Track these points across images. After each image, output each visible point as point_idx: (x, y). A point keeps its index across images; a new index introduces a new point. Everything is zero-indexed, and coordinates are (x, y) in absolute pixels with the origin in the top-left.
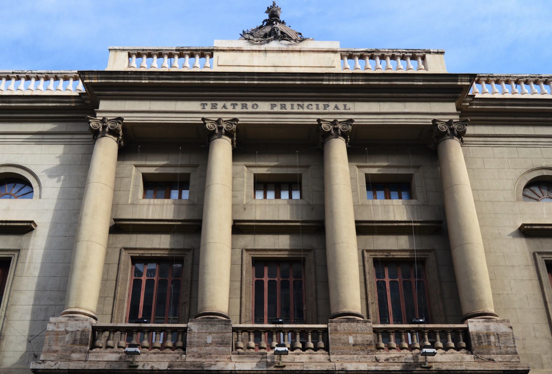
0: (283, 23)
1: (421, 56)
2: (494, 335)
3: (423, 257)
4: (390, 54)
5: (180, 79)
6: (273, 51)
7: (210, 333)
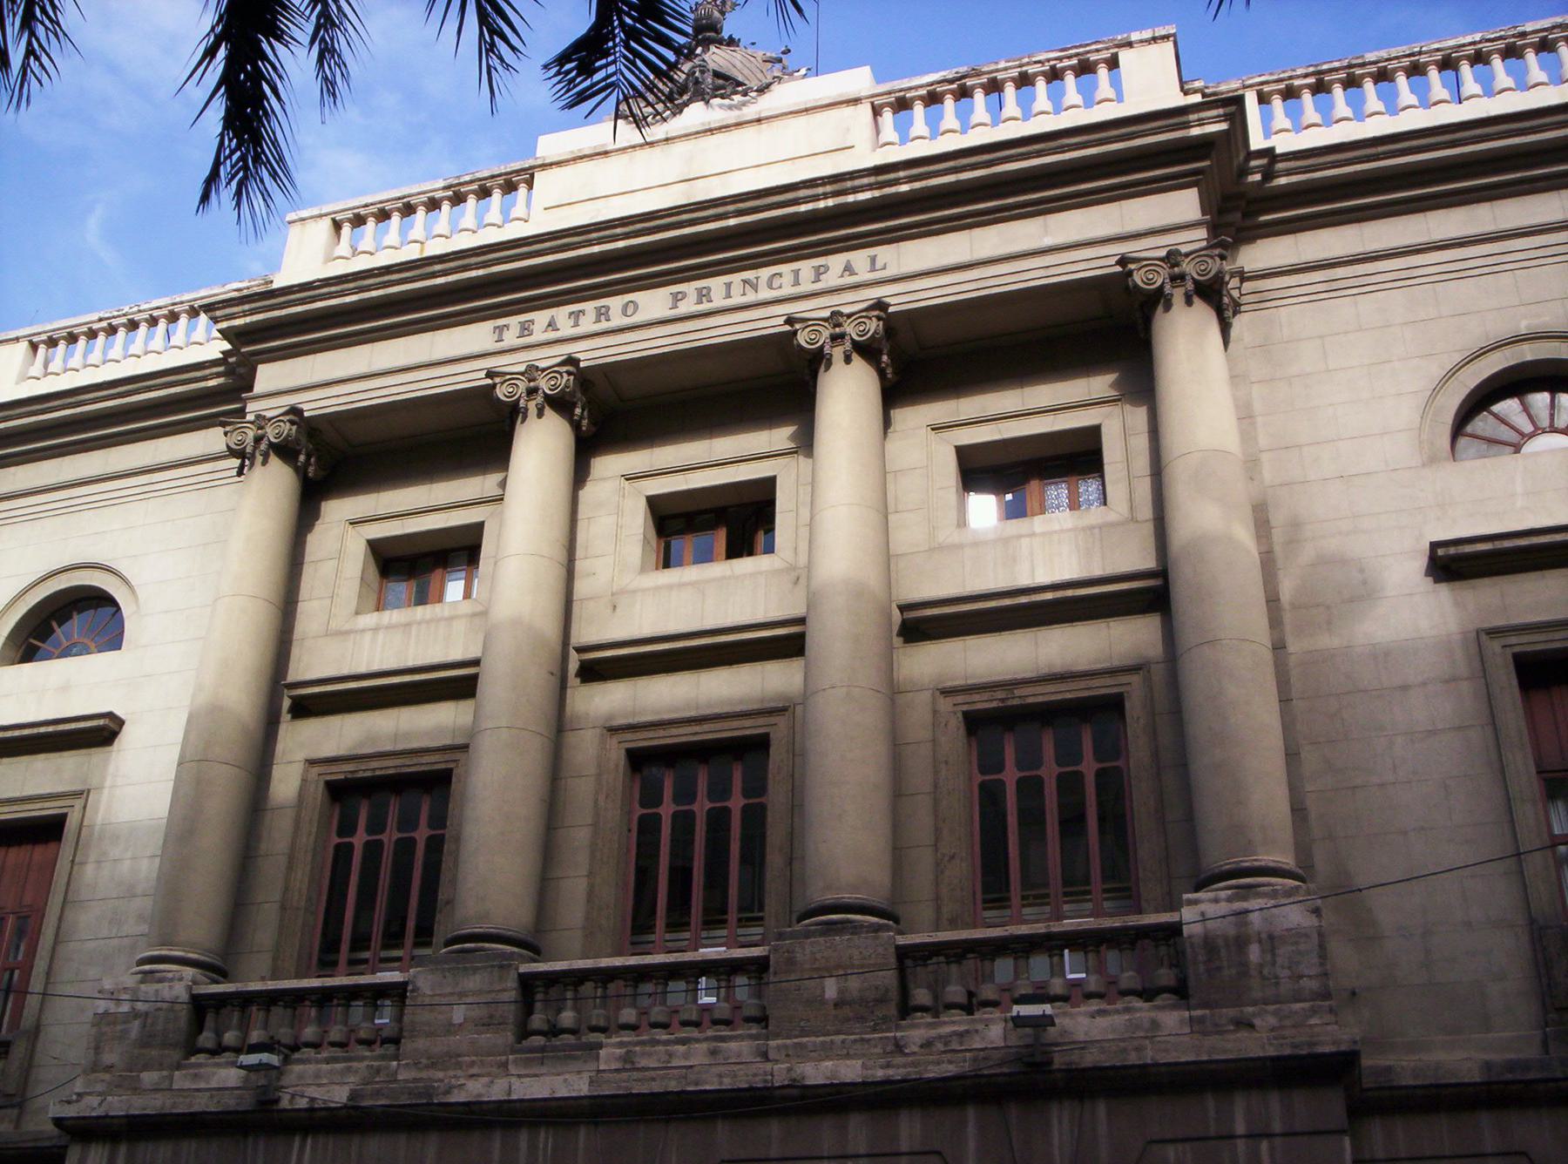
1: (1106, 61)
2: (1260, 942)
3: (443, 766)
5: (434, 275)
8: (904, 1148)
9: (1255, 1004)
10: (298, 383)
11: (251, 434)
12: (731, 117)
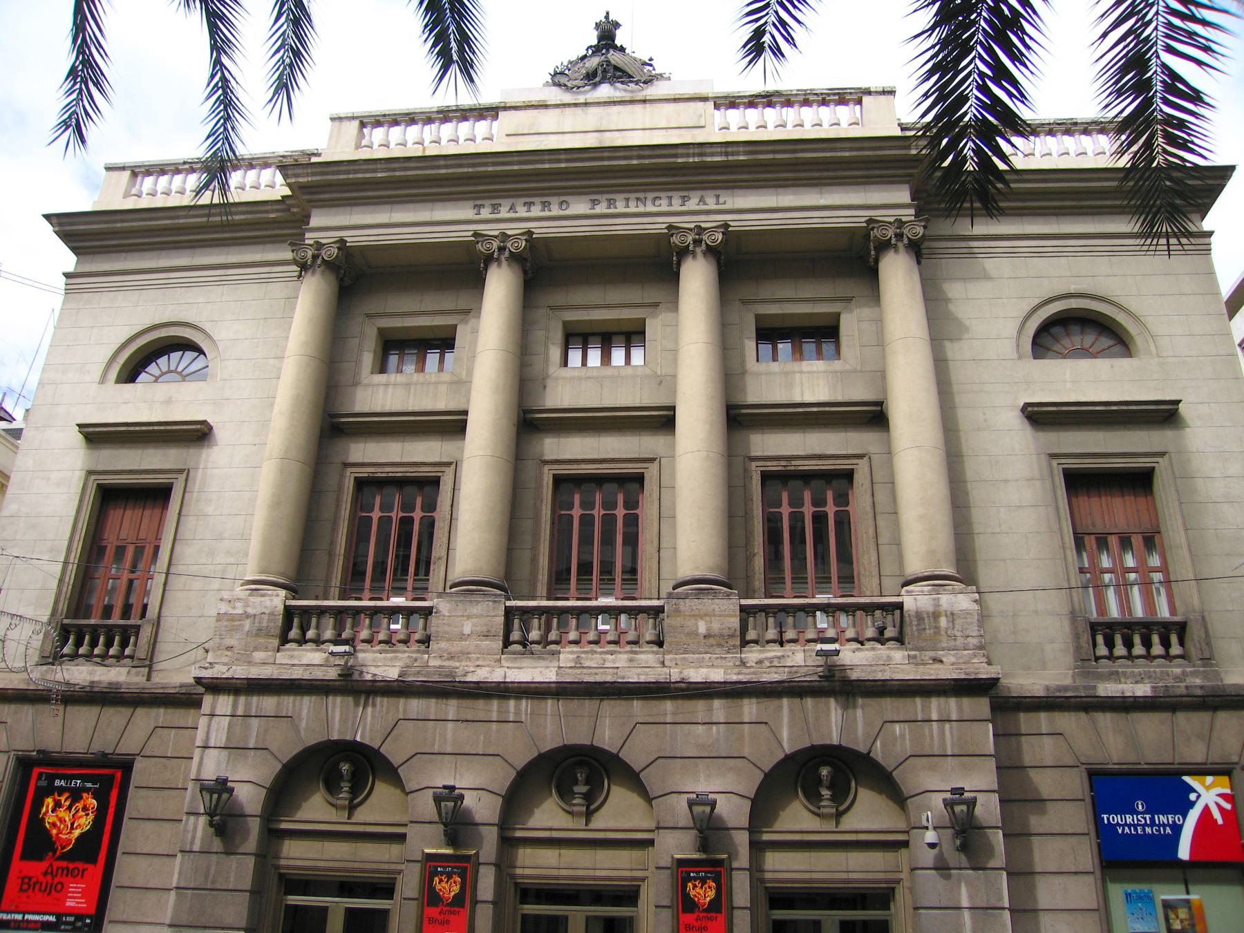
0: (622, 49)
4: (801, 98)
6: (599, 104)
7: (469, 617)
8: (746, 720)
10: (331, 225)
11: (310, 253)
12: (628, 96)
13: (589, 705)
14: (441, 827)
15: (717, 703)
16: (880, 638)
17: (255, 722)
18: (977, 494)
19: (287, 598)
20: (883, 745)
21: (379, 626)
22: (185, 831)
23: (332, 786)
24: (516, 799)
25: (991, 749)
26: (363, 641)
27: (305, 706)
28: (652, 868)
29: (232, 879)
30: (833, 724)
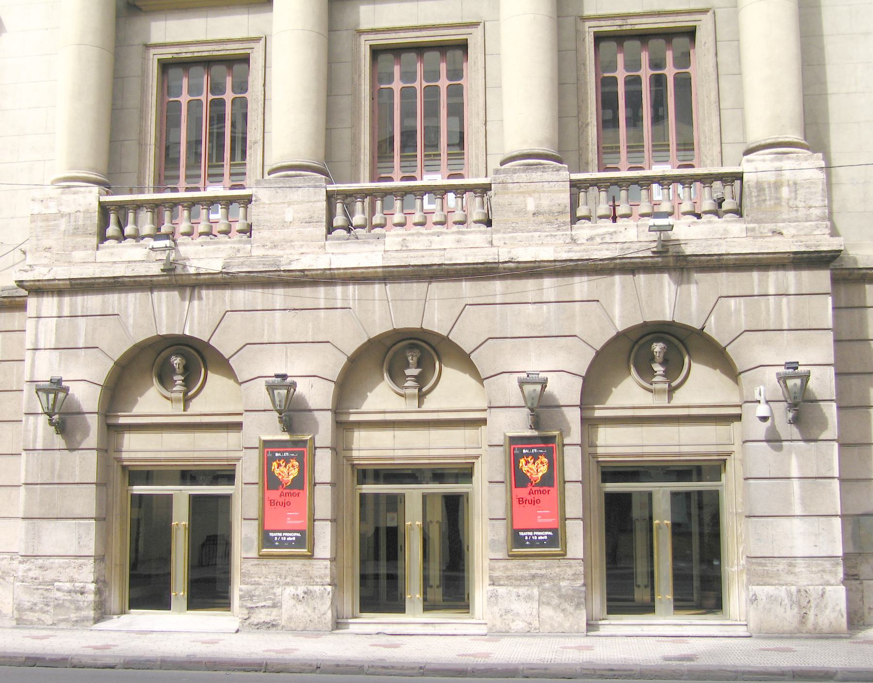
2: (789, 185)
7: (290, 204)
9: (784, 221)
13: (418, 288)
14: (277, 414)
15: (547, 282)
16: (718, 210)
17: (82, 321)
18: (835, 50)
19: (100, 194)
20: (716, 319)
21: (198, 215)
22: (26, 430)
23: (165, 379)
24: (349, 383)
25: (829, 323)
26: (184, 234)
27: (131, 303)
28: (485, 446)
29: (77, 473)
30: (666, 300)
